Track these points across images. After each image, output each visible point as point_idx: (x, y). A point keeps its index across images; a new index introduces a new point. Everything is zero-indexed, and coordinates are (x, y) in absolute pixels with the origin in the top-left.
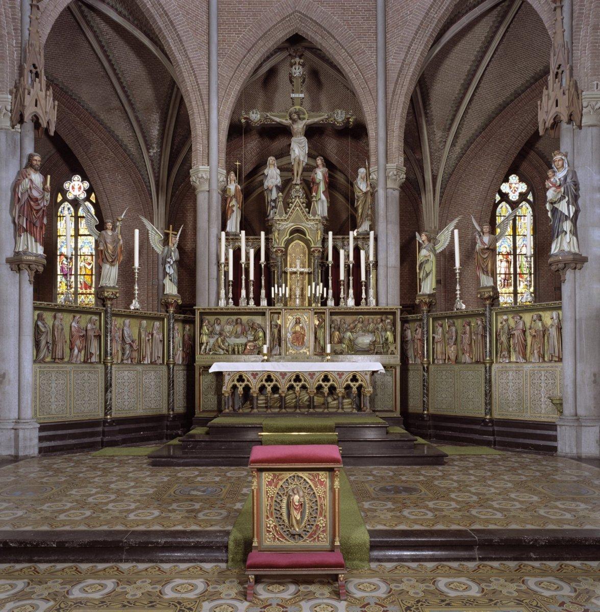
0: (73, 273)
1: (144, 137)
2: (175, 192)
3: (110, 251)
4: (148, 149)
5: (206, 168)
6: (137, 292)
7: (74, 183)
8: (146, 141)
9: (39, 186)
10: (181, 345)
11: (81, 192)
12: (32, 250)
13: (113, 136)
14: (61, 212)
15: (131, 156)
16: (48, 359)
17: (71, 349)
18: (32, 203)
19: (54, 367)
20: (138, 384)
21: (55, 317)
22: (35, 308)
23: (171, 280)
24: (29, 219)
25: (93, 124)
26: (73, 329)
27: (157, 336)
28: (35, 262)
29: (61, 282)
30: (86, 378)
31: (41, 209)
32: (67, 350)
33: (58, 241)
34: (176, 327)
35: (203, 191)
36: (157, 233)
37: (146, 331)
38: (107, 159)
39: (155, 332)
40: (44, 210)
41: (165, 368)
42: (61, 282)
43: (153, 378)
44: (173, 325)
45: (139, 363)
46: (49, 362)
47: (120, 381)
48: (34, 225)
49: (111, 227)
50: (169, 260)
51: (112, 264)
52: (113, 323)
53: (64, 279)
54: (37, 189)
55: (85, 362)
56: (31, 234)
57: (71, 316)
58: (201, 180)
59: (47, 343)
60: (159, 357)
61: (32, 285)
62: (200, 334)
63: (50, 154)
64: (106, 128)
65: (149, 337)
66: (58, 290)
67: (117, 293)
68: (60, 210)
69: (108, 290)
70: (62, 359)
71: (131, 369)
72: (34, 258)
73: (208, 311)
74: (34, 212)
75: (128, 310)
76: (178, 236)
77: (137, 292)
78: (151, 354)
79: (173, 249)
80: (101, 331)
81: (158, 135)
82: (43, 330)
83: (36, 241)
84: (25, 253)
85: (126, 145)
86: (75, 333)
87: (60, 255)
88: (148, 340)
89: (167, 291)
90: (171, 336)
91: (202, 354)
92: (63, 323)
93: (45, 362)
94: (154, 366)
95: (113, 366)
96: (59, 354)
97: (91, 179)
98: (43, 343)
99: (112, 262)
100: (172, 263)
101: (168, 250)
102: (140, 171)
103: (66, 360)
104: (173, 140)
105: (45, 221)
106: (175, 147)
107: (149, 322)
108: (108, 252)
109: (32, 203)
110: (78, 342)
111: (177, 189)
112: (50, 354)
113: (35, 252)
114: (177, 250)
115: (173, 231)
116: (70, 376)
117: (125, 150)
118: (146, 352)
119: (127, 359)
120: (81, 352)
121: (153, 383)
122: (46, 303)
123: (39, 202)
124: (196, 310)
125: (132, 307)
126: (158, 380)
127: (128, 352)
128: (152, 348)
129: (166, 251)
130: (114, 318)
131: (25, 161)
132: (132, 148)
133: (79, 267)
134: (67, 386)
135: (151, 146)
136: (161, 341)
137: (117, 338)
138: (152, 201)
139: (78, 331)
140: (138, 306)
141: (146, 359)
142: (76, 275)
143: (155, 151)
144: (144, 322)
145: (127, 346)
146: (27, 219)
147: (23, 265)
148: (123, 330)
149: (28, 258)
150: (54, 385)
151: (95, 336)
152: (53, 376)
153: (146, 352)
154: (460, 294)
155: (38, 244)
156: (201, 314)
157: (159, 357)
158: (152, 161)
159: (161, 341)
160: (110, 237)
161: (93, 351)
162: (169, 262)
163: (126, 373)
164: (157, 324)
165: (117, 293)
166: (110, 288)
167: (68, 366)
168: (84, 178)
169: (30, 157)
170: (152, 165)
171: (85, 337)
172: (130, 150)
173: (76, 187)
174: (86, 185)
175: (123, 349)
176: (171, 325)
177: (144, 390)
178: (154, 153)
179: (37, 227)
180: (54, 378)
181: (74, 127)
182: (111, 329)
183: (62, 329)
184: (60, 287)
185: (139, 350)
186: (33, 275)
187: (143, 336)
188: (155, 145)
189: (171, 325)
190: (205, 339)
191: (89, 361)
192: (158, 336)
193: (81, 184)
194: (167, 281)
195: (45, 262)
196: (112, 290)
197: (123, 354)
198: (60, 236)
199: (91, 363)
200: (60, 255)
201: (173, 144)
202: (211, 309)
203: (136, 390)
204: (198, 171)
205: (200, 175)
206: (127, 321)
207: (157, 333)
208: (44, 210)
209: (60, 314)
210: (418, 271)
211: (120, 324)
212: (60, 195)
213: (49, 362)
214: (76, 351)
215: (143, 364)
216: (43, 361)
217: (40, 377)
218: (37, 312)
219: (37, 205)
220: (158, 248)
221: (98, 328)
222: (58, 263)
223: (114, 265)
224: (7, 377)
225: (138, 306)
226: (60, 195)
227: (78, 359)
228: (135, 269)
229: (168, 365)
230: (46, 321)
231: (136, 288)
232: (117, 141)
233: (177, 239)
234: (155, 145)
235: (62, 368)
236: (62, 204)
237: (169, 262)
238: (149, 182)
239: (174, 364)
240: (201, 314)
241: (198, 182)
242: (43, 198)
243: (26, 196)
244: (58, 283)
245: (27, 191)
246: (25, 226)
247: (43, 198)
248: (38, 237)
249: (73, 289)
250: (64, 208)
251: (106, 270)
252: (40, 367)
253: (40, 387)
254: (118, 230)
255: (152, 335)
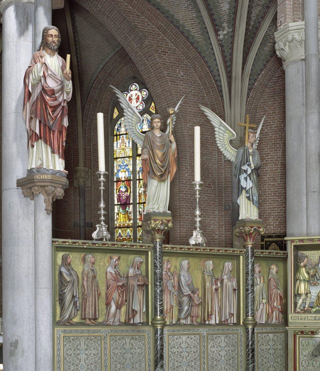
0: (131, 201)
1: (211, 15)
2: (253, 84)
3: (158, 161)
4: (216, 31)
5: (300, 24)
6: (198, 219)
7: (131, 93)
8: (213, 21)
9: (56, 73)
10: (265, 296)
11: (139, 103)
12: (48, 166)
13: (172, 22)
14: (118, 129)
15: (195, 45)
16: (76, 320)
17: (108, 304)
18: (47, 98)
19: (83, 332)
20: (202, 355)
21: (84, 260)
22: (58, 249)
23: (248, 198)
24: (43, 122)
25: (148, 10)
26: (109, 276)
27: (230, 283)
28: (52, 181)
29: (118, 214)
30: (127, 346)
31: (60, 104)
32: (102, 306)
33: (115, 165)
34: (257, 269)
35: (295, 62)
36: (227, 129)
37: (213, 276)
38: (165, 53)
39: (225, 277)
40: (63, 107)
41: (241, 330)
42: (118, 214)
43: (223, 344)
44: (253, 265)
45: (203, 324)
46: (77, 324)
47: (175, 350)
48: (50, 129)
49: (159, 124)
50: (245, 167)
51: (162, 178)
52: (165, 266)
53: (121, 210)
54: (53, 76)
55: (127, 323)
56: (46, 142)
57: (107, 257)
58: (292, 44)
59: (73, 297)
60: (231, 315)
61: (50, 217)
62: (296, 280)
63: (104, 63)
64: (163, 13)
65: (216, 284)
66: (116, 223)
67: (169, 221)
68: (116, 127)
69: (155, 218)
70: (95, 319)
71: (191, 332)
72: (50, 177)
73: (308, 243)
74: (50, 110)
75: (186, 247)
76: (259, 131)
77: (198, 219)
78: (220, 309)
79: (250, 151)
80: (148, 278)
81: (229, 9)
82: (68, 279)
83: (53, 152)
84: (39, 170)
85: (188, 31)
86: (111, 282)
87: (117, 182)
88: (216, 290)
89: (243, 215)
90: (250, 282)
91: (298, 313)
92: (96, 267)
93: (72, 325)
94: (226, 328)
95: (166, 329)
96: (90, 312)
97: (149, 86)
98: (68, 297)
99: (161, 176)
100: (249, 171)
101: (244, 152)
102: (206, 62)
103: (100, 320)
104: (249, 13)
105: (66, 123)
106: (252, 23)
107: (217, 261)
108: (156, 163)
109: (47, 98)
110: (115, 295)
111: (255, 80)
112: (79, 313)
113: (51, 168)
114: (256, 151)
115: (250, 122)
116: (105, 343)
117: (187, 38)
118: (212, 307)
119: (186, 318)
120: (120, 309)
121: (223, 353)
122: (70, 241)
123: (57, 95)
124: (289, 243)
125: (192, 242)
126: (232, 348)
127: (186, 308)
128: (222, 300)
129: (240, 155)
130: (165, 258)
131: (39, 40)
132: (196, 34)
133: (138, 194)
134: (101, 358)
135: (221, 26)
136: (235, 290)
137: (170, 288)
138: (223, 100)
139: (116, 280)
140: (200, 240)
141: (213, 316)
142: (135, 204)
143: (225, 32)
144: (210, 264)
145: (185, 299)
146: (40, 122)
147: (36, 188)
148: (179, 276)
149: (43, 177)
150: (83, 357)
151: (138, 285)
152: (82, 343)
153: (212, 307)
154: (200, 222)
155: (56, 156)
156: (297, 248)
157: (231, 315)
158: (221, 46)
159: (235, 290)
160: (158, 140)
161: (136, 307)
162: (246, 171)
163: (184, 338)
164: (228, 265)
165: (169, 221)
166: (159, 214)
167: (103, 329)
168: (143, 86)
169: (45, 31)
170: (223, 52)
171: (125, 288)
172: (193, 37)
173: (134, 97)
174: (145, 93)
175: (180, 304)
176: (250, 266)
177: (210, 363)
178: (224, 35)
179: (54, 131)
180: (83, 346)
181: (125, 18)
182: (161, 274)
183: (94, 277)
184: (117, 219)
185: (203, 304)
186: (51, 201)
187: (208, 284)
188: (225, 25)
189: (250, 266)
190: (302, 288)
191: (132, 322)
192: (230, 284)
193: (139, 93)
194: (242, 201)
195: (65, 181)
196: (160, 218)
197: (180, 311)
198: (117, 158)
199: (134, 324)
200: (117, 182)
201: (249, 18)
202: (312, 240)
203: (198, 363)
204: (288, 31)
205: (290, 37)
206: (185, 263)
207: (229, 279)
208: (63, 107)
209: (90, 256)
210: (138, 233)
211: (176, 267)
212: (116, 110)
213: (77, 324)
214: (113, 308)
215: (209, 325)
216: (69, 323)
217: (64, 346)
218: (60, 255)
219: (54, 100)
220: (230, 153)
221: (144, 274)
222: (115, 191)
223: (164, 181)
224: (19, 346)
225: (200, 240)
226: (116, 110)
227: (116, 320)
228: (195, 185)
229: (245, 325)
230: (73, 266)
231: (198, 213)
232: (178, 27)
233: (257, 135)
234: (225, 25)
235: (94, 332)
236: (118, 121)
237: (246, 171)
238: (219, 75)
239: (255, 324)
240: (297, 248)
241: (287, 49)
242: (62, 89)
243: (39, 89)
244: (116, 214)
245: (41, 80)
246: (38, 132)
247: (62, 89)
248: (56, 147)
249: (132, 221)
250: (120, 124)
251: (153, 188)
252: (65, 332)
253: (65, 359)
254: (169, 129)
255: (222, 281)
